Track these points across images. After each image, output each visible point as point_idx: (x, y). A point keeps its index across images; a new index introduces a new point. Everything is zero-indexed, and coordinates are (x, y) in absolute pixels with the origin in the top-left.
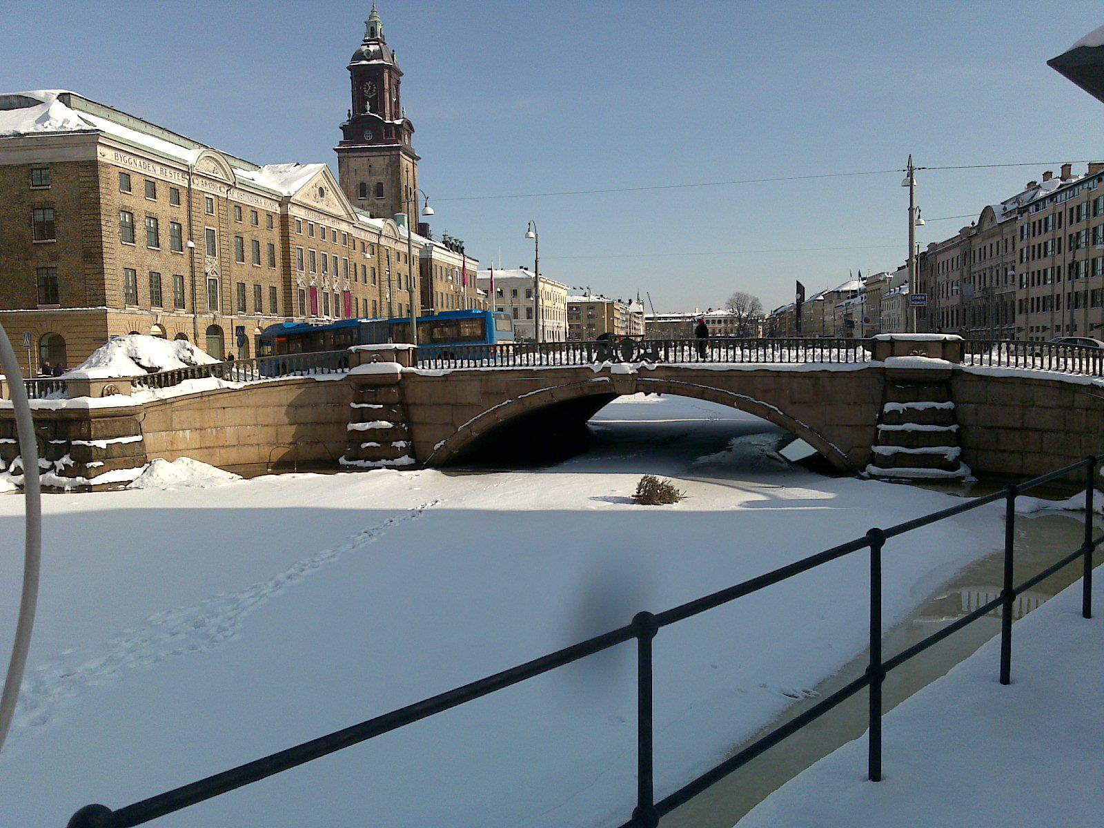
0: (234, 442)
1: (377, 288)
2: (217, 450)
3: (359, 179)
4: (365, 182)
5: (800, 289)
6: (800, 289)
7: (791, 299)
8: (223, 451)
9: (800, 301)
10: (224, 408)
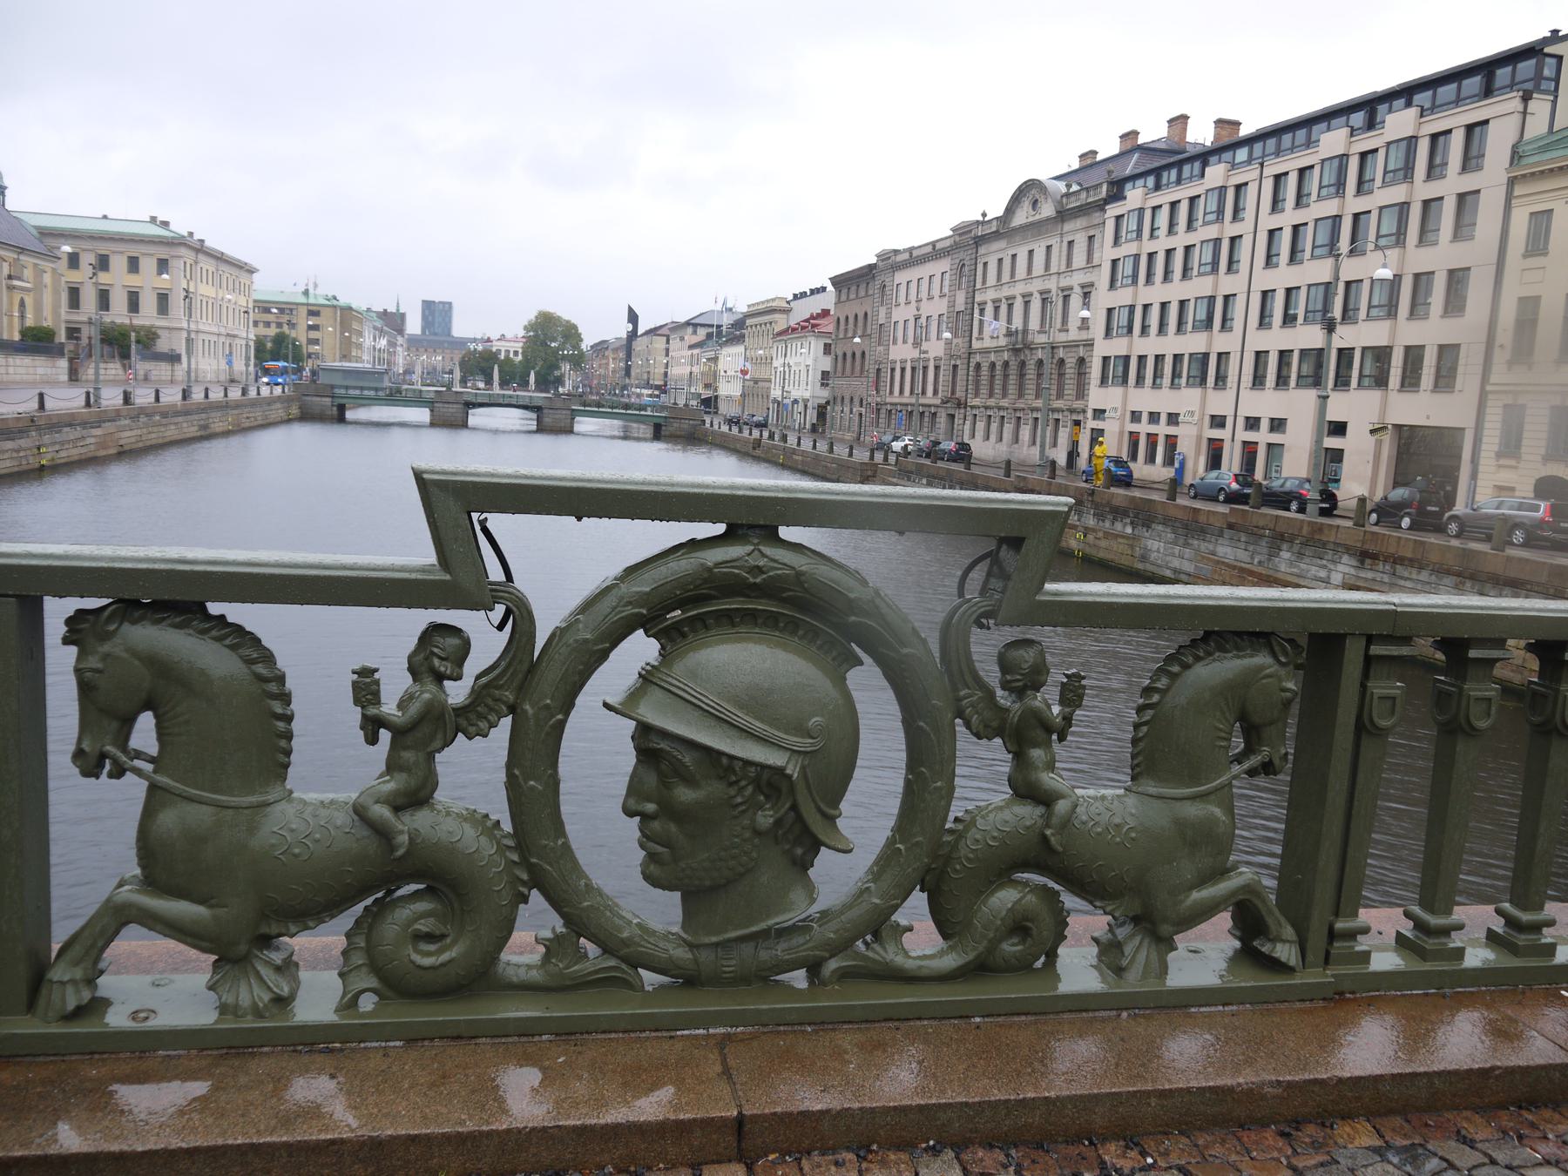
5: (633, 317)
6: (633, 317)
7: (622, 329)
9: (633, 335)
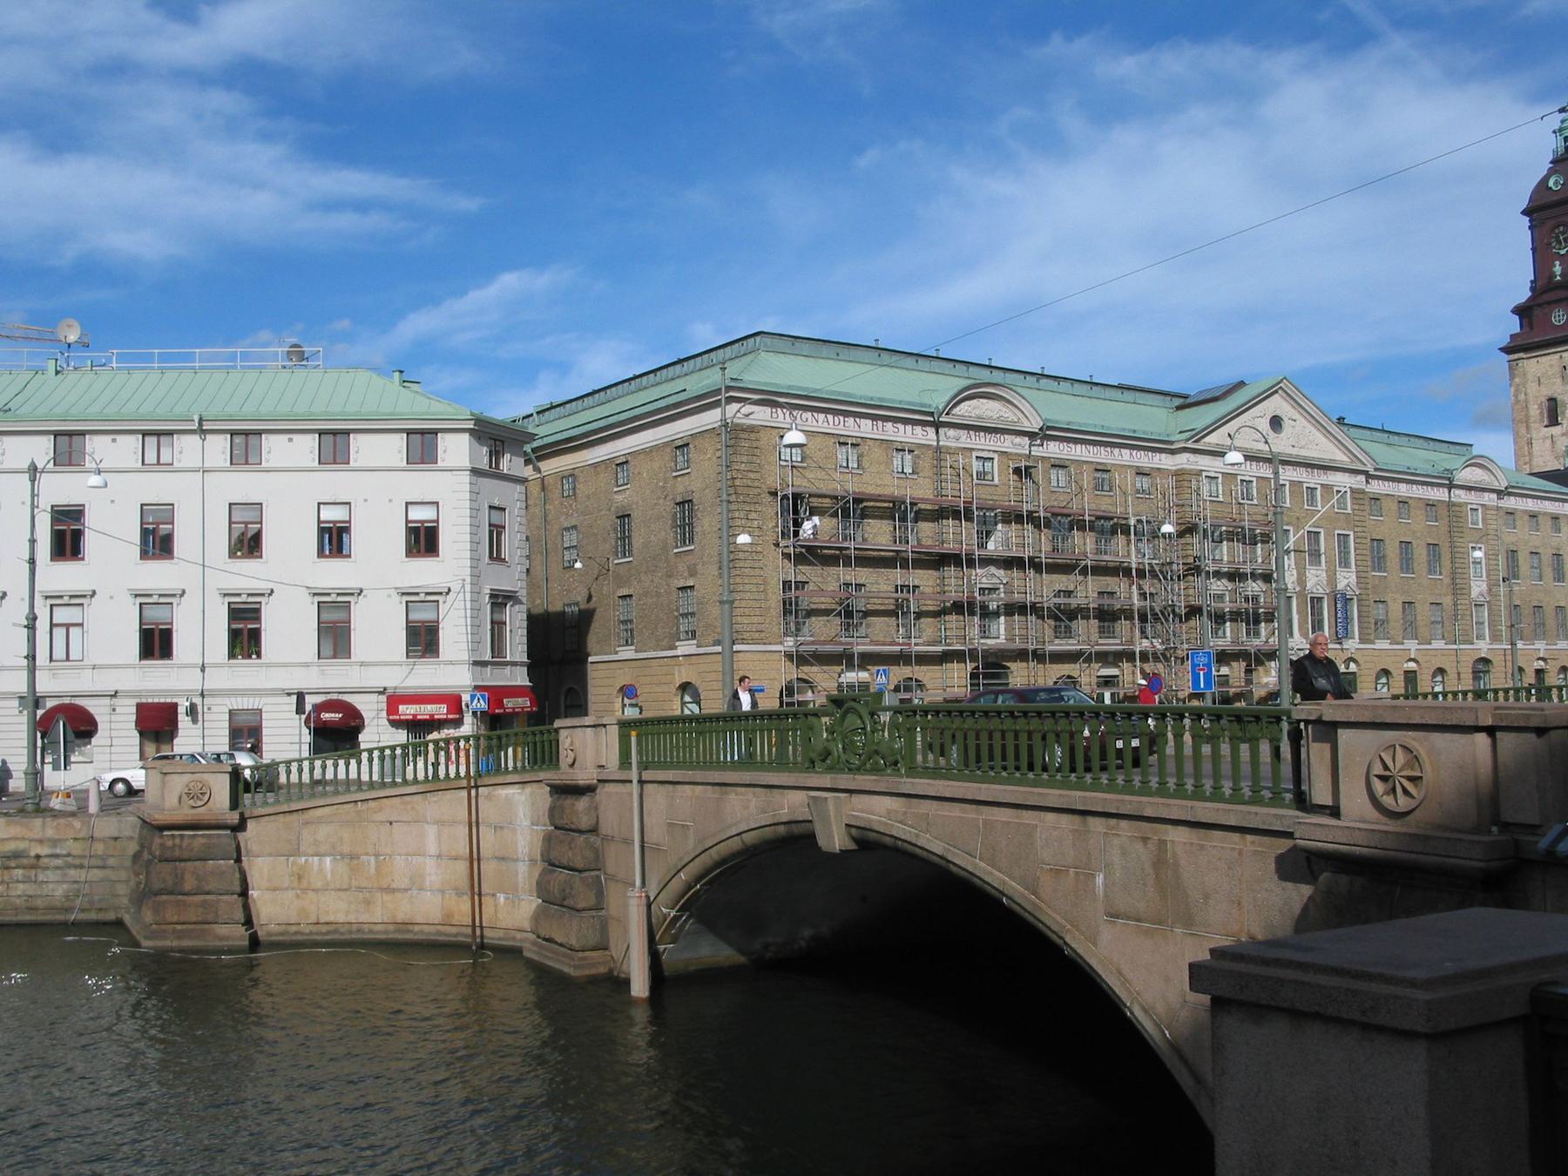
0: (405, 883)
1: (1447, 581)
2: (379, 895)
3: (1547, 392)
4: (1555, 396)
8: (387, 897)
10: (391, 823)
